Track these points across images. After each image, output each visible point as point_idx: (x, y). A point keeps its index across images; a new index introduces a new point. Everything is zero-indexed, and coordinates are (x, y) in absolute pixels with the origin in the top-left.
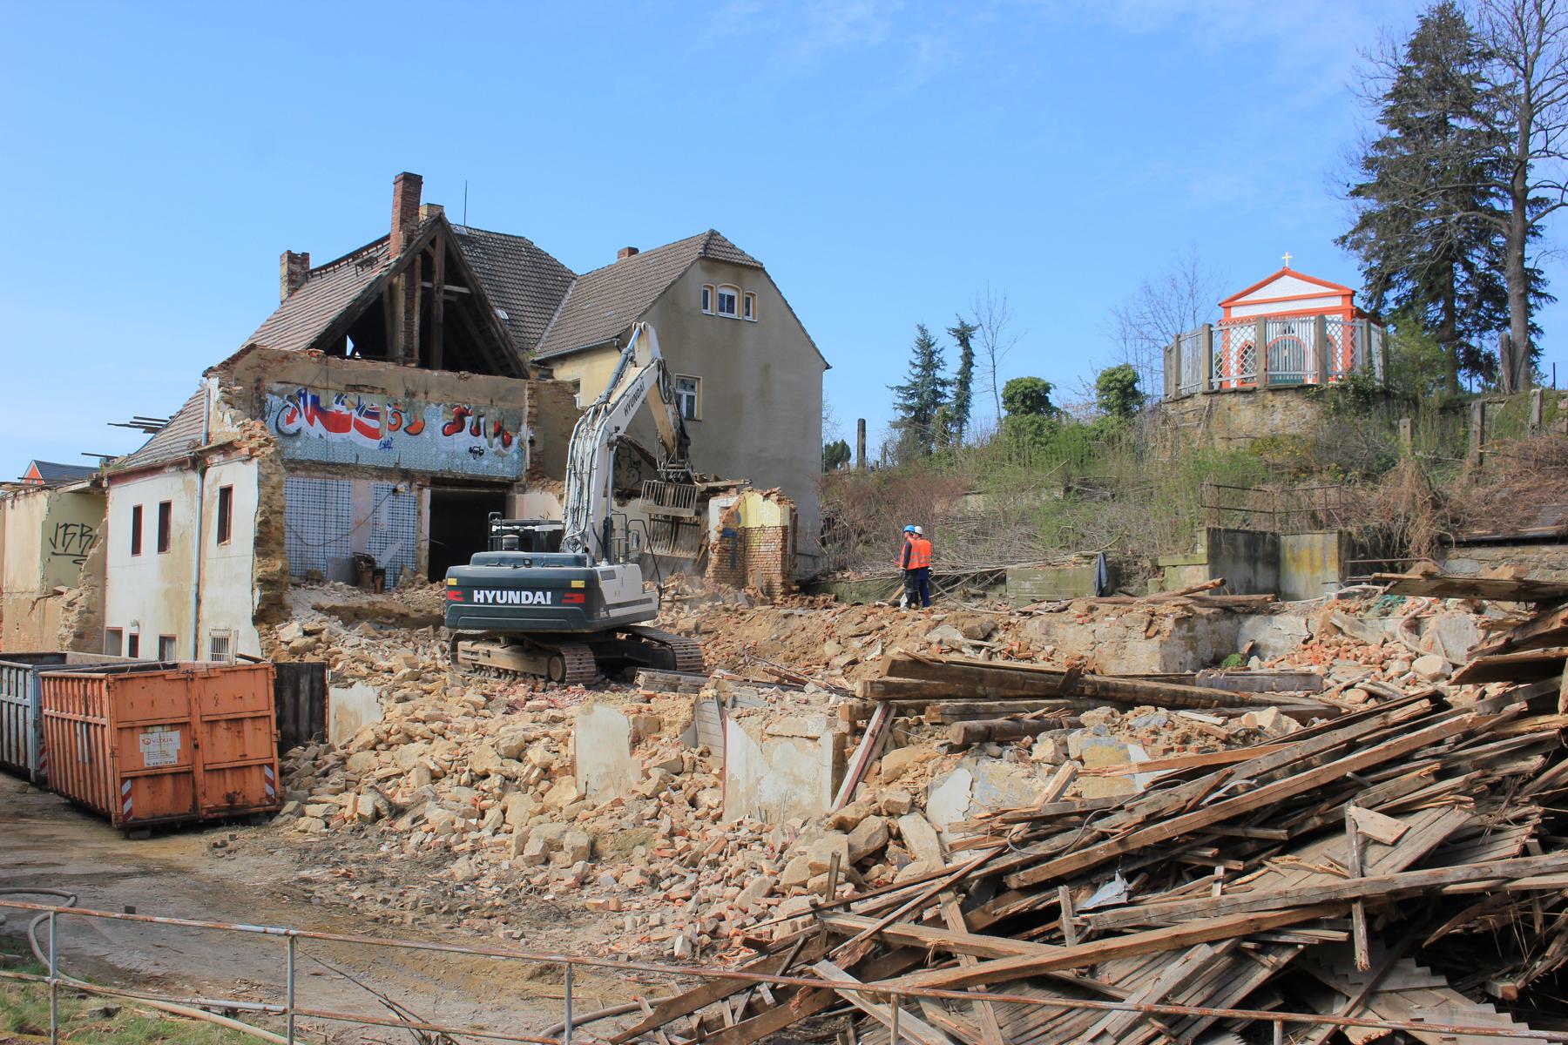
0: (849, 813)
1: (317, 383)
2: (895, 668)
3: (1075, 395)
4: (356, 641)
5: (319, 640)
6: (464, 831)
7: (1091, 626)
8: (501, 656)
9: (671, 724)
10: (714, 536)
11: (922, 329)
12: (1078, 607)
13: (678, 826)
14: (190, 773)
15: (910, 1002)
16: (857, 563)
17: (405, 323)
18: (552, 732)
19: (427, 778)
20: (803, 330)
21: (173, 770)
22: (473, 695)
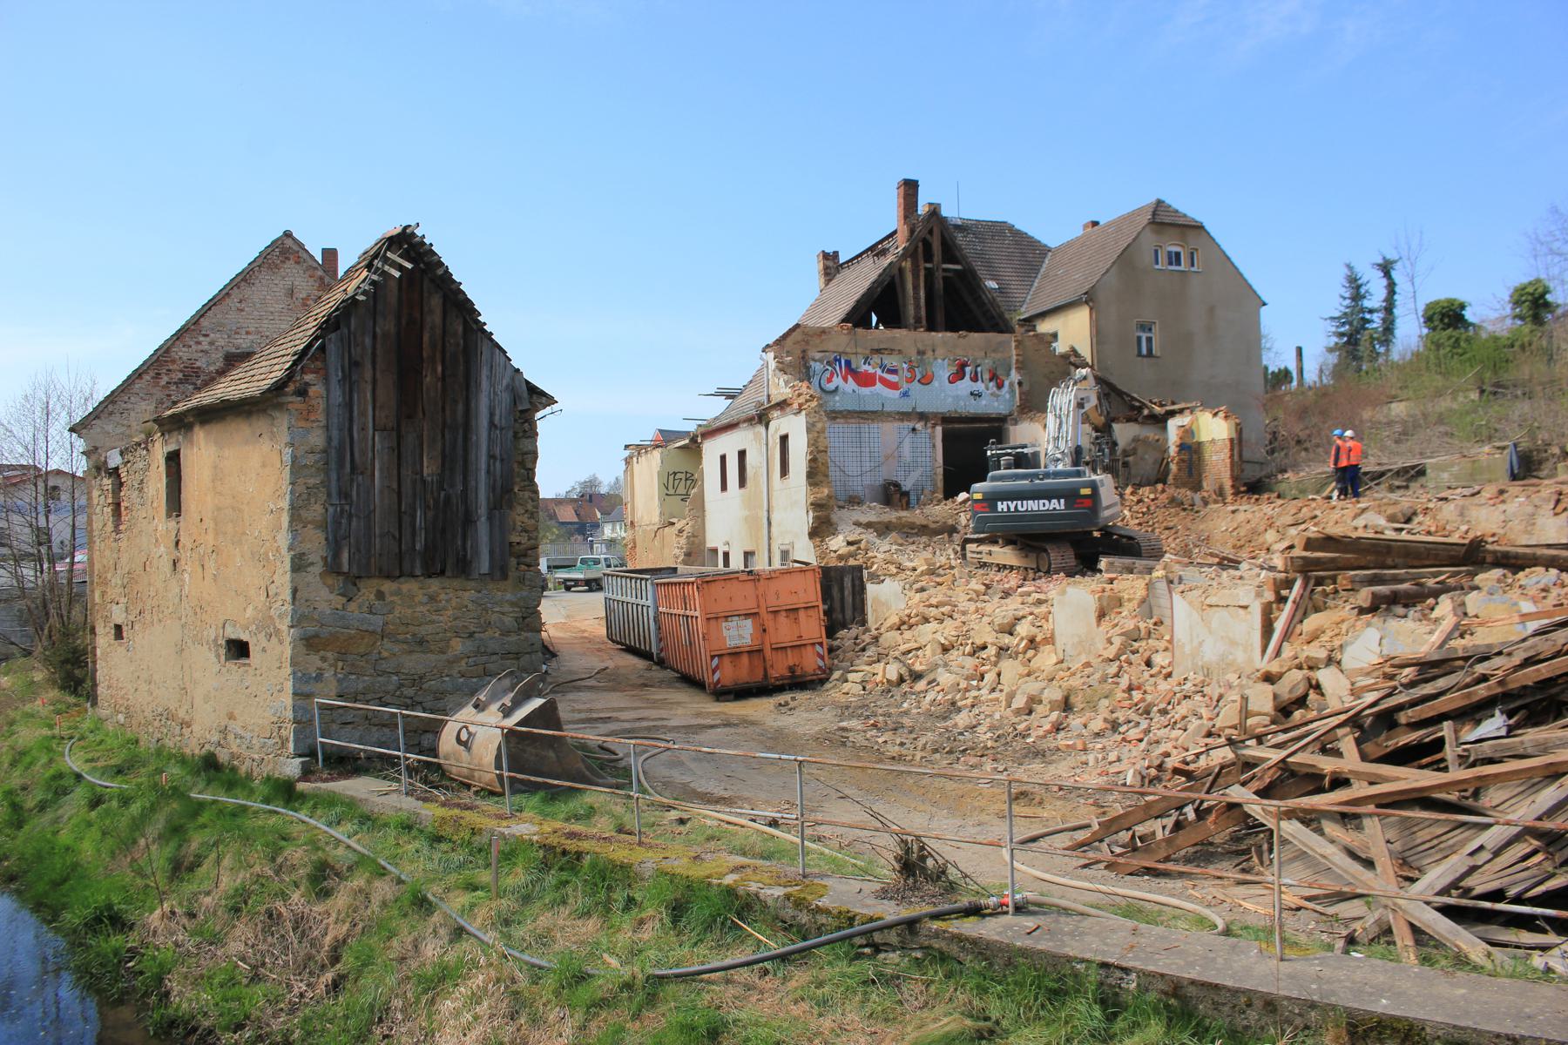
0: (1274, 668)
2: (1310, 544)
3: (1489, 309)
4: (887, 547)
6: (967, 690)
7: (1502, 507)
8: (1004, 554)
9: (1129, 600)
10: (1173, 450)
11: (1349, 267)
12: (1489, 491)
13: (1135, 683)
15: (1310, 819)
16: (1295, 466)
17: (913, 297)
18: (1036, 611)
22: (975, 585)
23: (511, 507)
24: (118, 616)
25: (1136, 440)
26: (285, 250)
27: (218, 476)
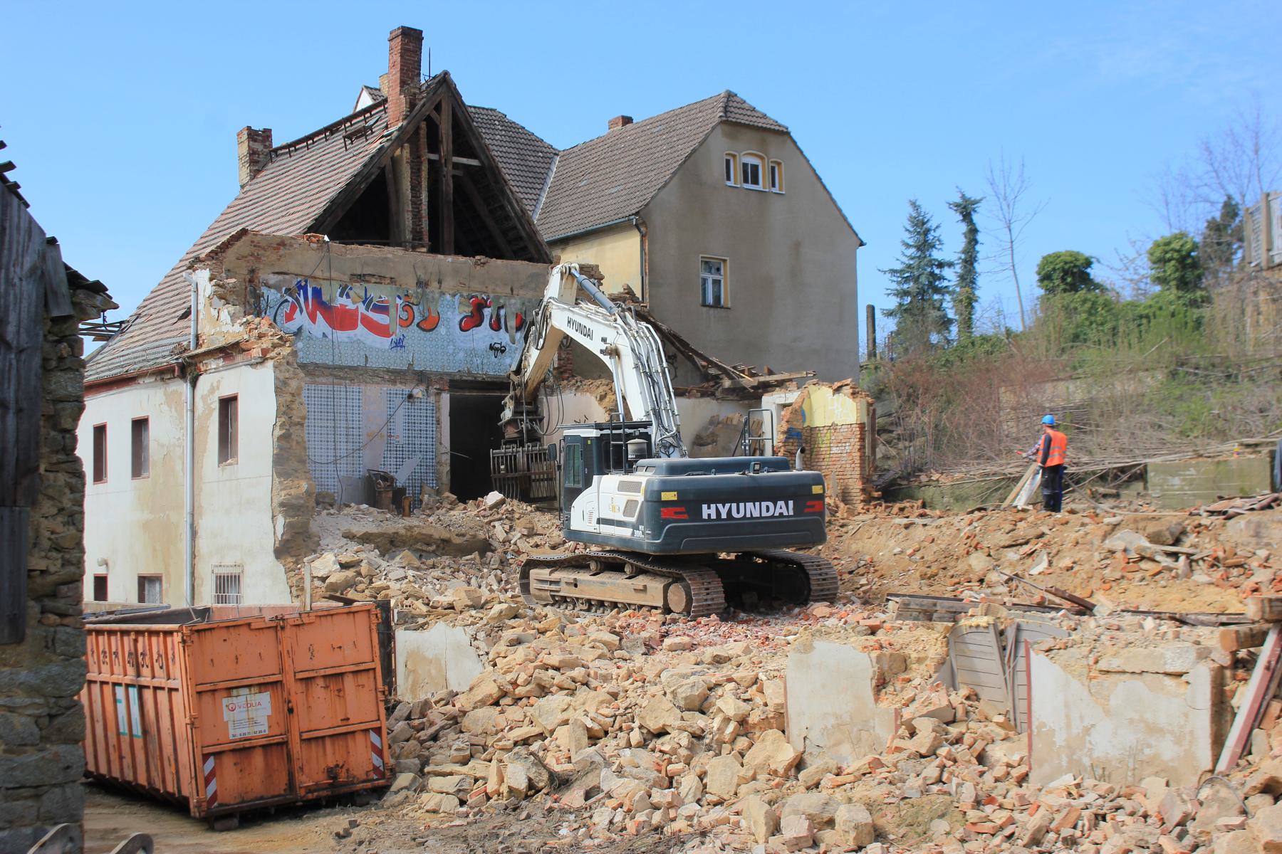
1: (318, 273)
3: (1123, 270)
4: (401, 573)
5: (359, 574)
9: (920, 661)
11: (915, 205)
14: (284, 744)
19: (585, 740)
20: (834, 202)
21: (263, 742)
23: (34, 503)
25: (714, 422)
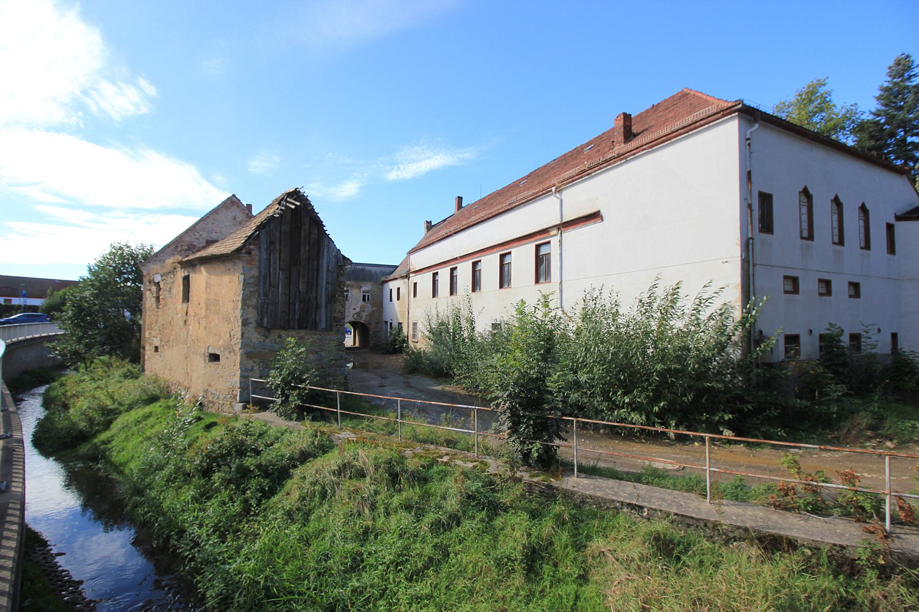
24: (157, 342)
26: (232, 202)
27: (208, 286)
